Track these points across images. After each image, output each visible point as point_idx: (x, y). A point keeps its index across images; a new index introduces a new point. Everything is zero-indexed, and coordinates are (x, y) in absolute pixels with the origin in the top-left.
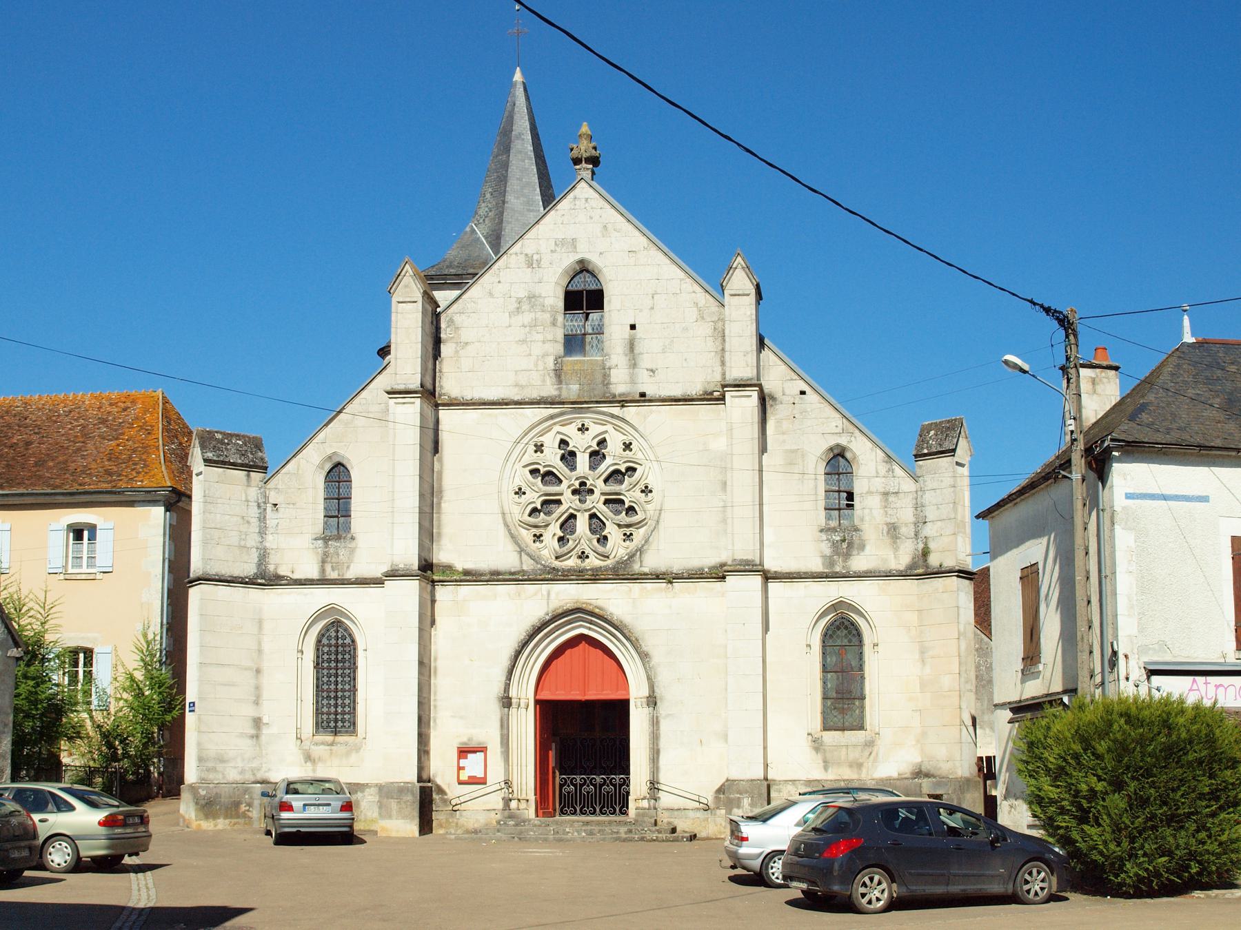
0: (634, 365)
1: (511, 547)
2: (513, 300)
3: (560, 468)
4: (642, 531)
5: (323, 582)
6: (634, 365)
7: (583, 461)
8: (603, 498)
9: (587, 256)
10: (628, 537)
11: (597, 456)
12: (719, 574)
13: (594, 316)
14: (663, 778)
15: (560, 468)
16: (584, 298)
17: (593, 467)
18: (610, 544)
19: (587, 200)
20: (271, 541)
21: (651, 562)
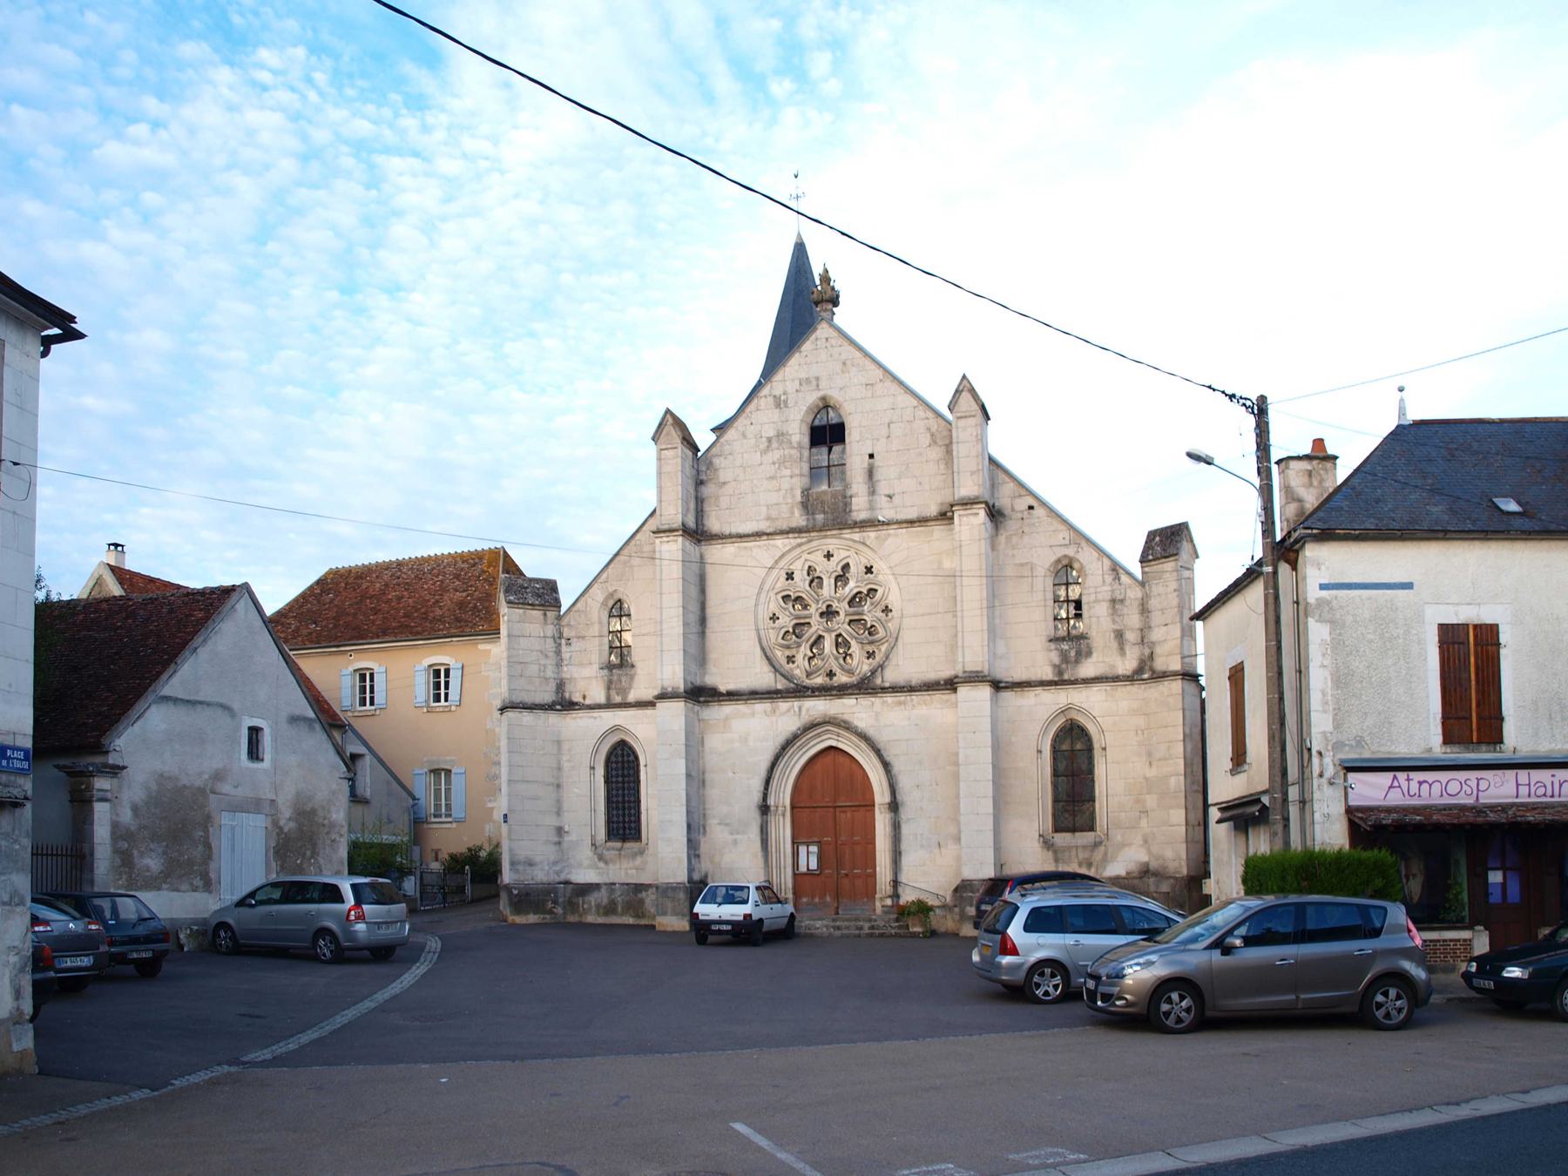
0: (872, 492)
1: (766, 668)
4: (883, 648)
5: (609, 705)
6: (872, 492)
7: (828, 583)
9: (829, 393)
12: (951, 685)
13: (837, 449)
14: (903, 878)
20: (568, 672)
21: (891, 676)
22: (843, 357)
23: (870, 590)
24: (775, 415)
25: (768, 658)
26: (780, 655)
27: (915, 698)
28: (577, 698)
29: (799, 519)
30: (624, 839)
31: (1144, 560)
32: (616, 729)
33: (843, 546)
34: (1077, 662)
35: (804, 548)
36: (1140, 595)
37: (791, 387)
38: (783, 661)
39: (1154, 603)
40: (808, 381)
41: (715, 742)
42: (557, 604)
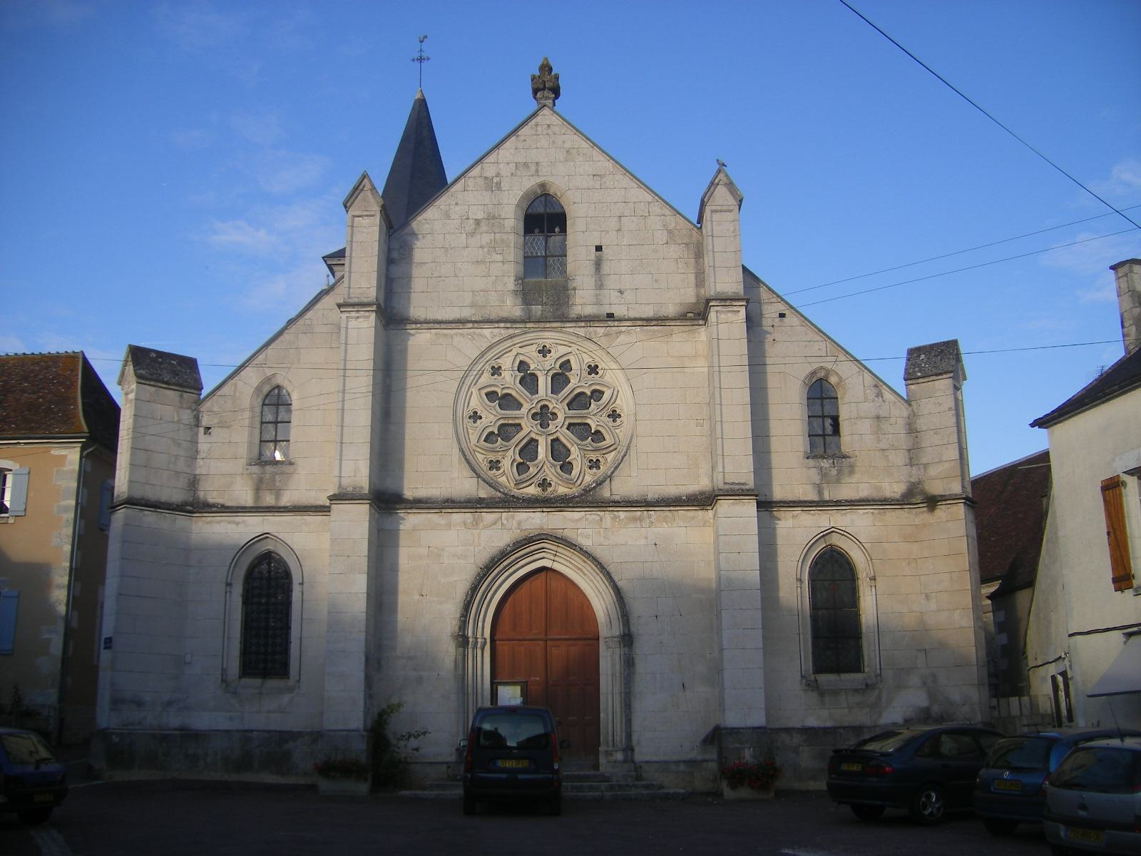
0: (600, 286)
1: (467, 472)
2: (471, 221)
3: (518, 391)
4: (610, 457)
6: (600, 286)
7: (544, 383)
8: (567, 423)
9: (551, 179)
10: (595, 464)
11: (559, 380)
12: (705, 500)
13: (555, 239)
15: (518, 391)
16: (544, 218)
17: (555, 389)
18: (575, 472)
19: (549, 126)
20: (201, 467)
21: (622, 487)
22: (567, 145)
23: (594, 391)
24: (486, 197)
25: (468, 462)
26: (481, 459)
27: (654, 514)
28: (213, 498)
29: (513, 307)
30: (265, 674)
31: (909, 377)
32: (264, 537)
33: (563, 344)
34: (838, 481)
35: (516, 340)
36: (905, 414)
37: (505, 170)
38: (485, 466)
39: (921, 424)
40: (526, 165)
41: (408, 558)
42: (199, 387)
